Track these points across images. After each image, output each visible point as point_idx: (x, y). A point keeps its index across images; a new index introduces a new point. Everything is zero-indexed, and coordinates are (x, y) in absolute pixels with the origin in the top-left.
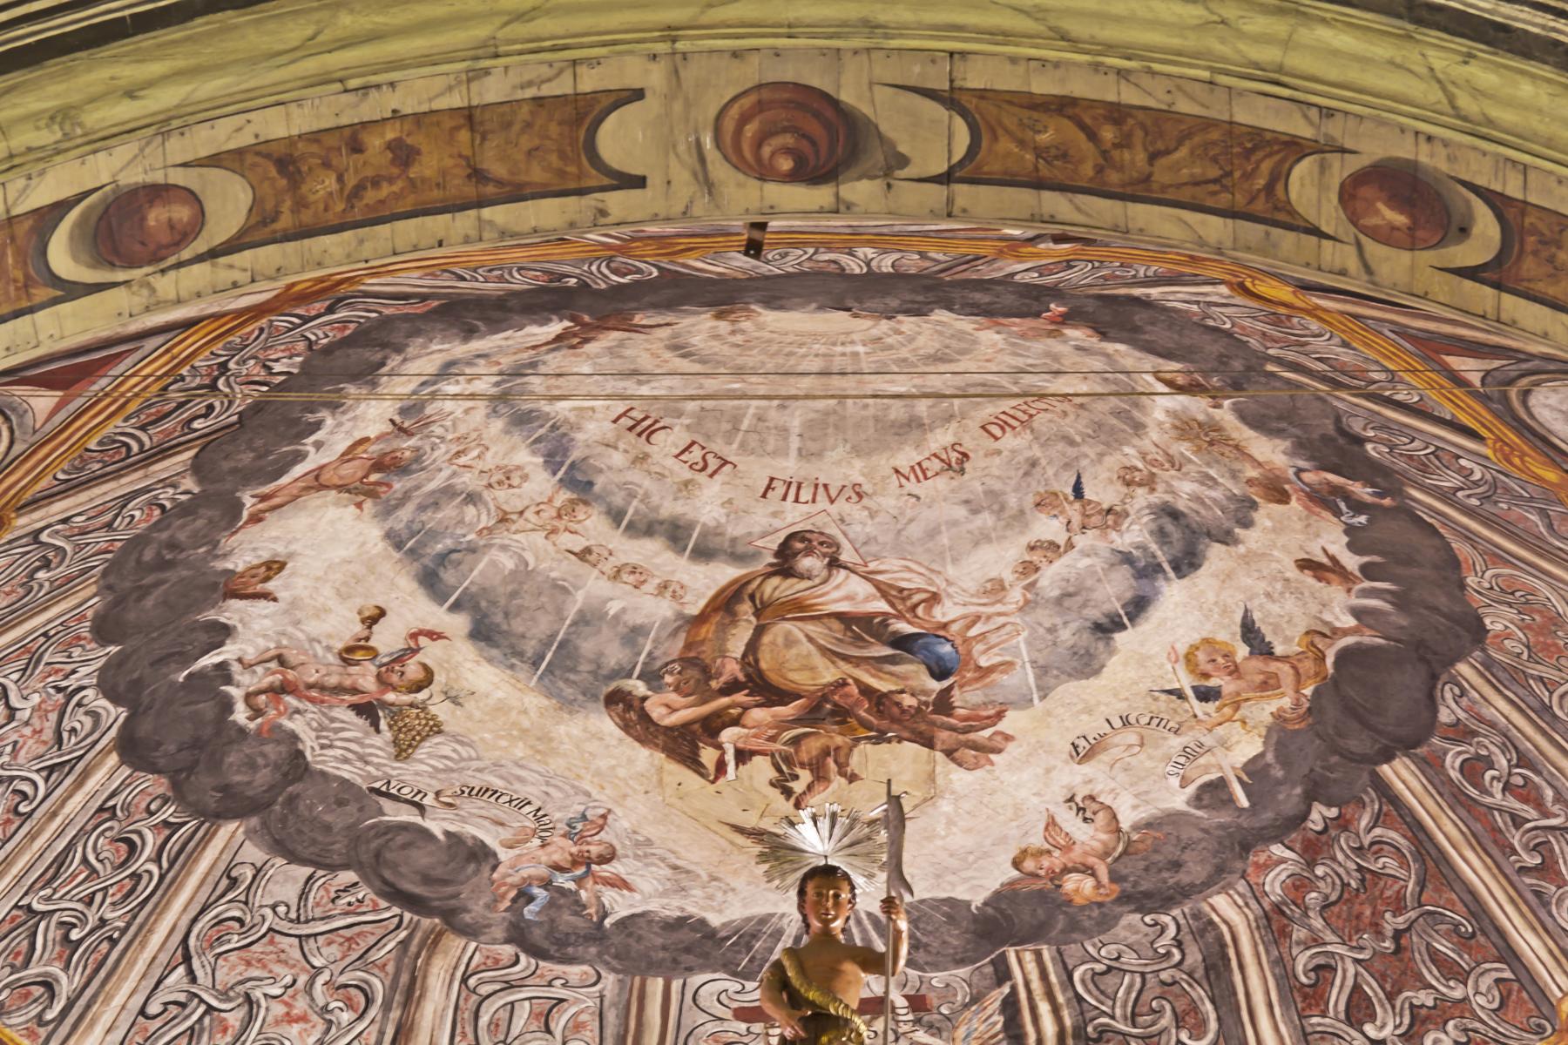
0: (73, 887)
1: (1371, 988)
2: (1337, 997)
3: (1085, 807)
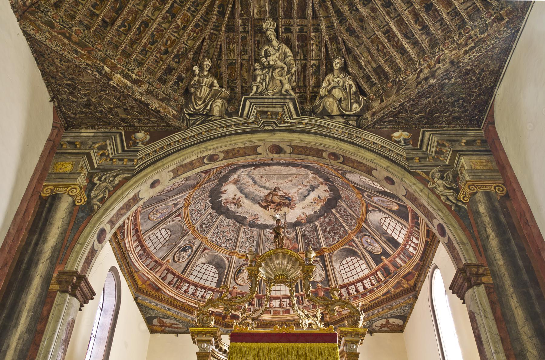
1: (331, 231)
2: (327, 231)
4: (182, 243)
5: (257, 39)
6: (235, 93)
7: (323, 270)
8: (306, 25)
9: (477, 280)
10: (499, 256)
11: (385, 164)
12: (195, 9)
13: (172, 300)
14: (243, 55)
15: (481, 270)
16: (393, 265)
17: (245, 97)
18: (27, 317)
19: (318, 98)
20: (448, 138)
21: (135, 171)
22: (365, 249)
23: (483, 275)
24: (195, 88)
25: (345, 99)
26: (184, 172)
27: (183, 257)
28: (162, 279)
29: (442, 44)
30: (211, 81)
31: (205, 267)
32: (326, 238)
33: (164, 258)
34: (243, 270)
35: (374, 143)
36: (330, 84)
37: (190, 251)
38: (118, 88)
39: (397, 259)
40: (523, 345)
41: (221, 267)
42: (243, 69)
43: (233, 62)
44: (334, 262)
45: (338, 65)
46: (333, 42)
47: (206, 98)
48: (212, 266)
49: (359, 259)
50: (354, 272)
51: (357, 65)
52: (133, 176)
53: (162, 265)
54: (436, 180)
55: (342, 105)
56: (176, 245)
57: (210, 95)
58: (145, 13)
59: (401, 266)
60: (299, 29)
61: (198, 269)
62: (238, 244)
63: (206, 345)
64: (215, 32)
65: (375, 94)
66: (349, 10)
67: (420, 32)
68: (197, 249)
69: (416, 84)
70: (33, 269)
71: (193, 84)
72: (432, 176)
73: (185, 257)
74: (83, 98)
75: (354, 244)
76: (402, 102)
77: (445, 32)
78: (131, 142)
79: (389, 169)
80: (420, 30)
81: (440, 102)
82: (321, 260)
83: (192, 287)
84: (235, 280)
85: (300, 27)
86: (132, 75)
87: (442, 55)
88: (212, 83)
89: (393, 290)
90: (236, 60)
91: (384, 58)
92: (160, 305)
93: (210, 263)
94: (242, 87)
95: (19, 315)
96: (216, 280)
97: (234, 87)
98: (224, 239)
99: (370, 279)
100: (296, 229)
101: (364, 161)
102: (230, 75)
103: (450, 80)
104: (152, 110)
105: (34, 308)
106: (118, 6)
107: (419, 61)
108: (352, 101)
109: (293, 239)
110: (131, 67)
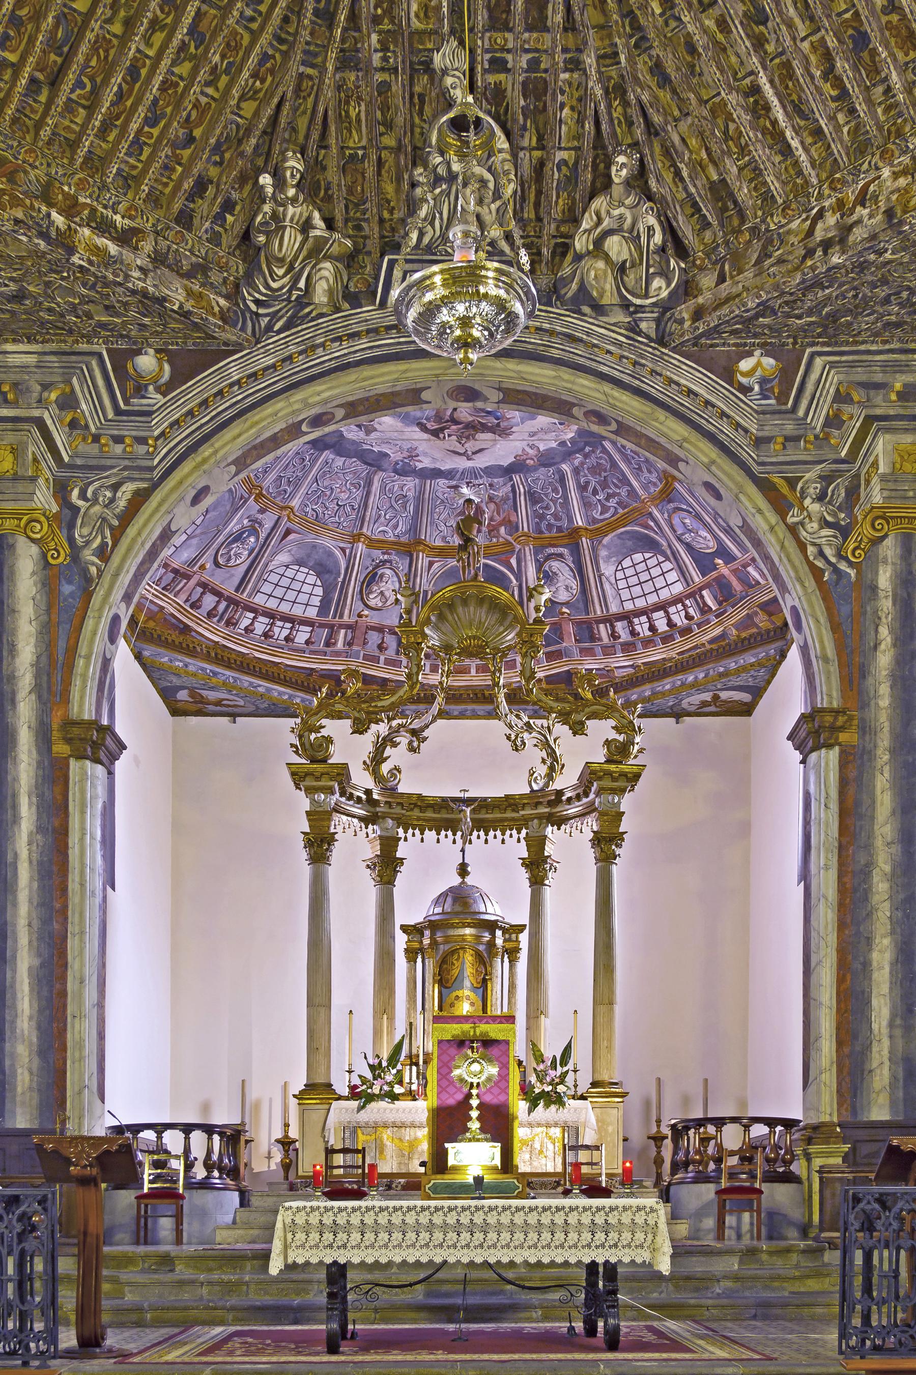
0: (291, 469)
1: (598, 487)
2: (590, 489)
3: (532, 447)
4: (233, 526)
5: (417, 89)
6: (365, 238)
7: (575, 578)
8: (546, 51)
9: (830, 738)
10: (884, 690)
11: (706, 455)
12: (255, 11)
13: (219, 651)
14: (381, 135)
15: (841, 720)
16: (739, 579)
17: (391, 257)
18: (30, 804)
19: (569, 258)
20: (863, 378)
21: (155, 473)
22: (679, 539)
23: (842, 729)
24: (268, 234)
25: (633, 265)
26: (260, 457)
27: (237, 555)
28: (192, 607)
29: (878, 153)
30: (305, 215)
31: (290, 573)
32: (587, 505)
33: (192, 562)
34: (382, 576)
35: (690, 392)
36: (600, 221)
37: (252, 539)
38: (92, 269)
39: (750, 569)
40: (871, 856)
41: (329, 572)
42: (383, 172)
43: (357, 154)
44: (601, 562)
45: (624, 172)
46: (615, 99)
47: (296, 258)
48: (306, 570)
49: (661, 559)
50: (648, 587)
51: (672, 169)
52: (155, 486)
53: (188, 577)
54: (807, 502)
55: (625, 278)
56: (219, 532)
57: (304, 253)
58: (130, 49)
59: (758, 583)
60: (529, 62)
61: (274, 578)
62: (368, 514)
63: (323, 796)
64: (310, 71)
65: (708, 255)
66: (661, 15)
67: (833, 105)
68: (269, 534)
69: (803, 252)
70: (11, 713)
71: (261, 224)
72: (803, 491)
73: (241, 555)
74: (6, 285)
75: (652, 524)
76: (764, 297)
77: (892, 113)
78: (130, 385)
79: (713, 468)
80: (834, 99)
81: (855, 296)
82: (572, 555)
83: (261, 619)
84: (362, 599)
85: (530, 56)
86: (115, 217)
87: (873, 181)
88: (309, 219)
89: (734, 632)
90: (364, 148)
91: (739, 160)
92: (195, 665)
93: (301, 563)
94: (381, 221)
95: (14, 801)
96: (316, 601)
97: (361, 220)
98: (333, 506)
99: (684, 605)
100: (511, 479)
101: (662, 441)
102: (350, 191)
103: (880, 253)
104: (173, 310)
105: (36, 788)
106: (59, 35)
107: (820, 187)
108: (651, 270)
109: (505, 499)
110: (110, 198)
